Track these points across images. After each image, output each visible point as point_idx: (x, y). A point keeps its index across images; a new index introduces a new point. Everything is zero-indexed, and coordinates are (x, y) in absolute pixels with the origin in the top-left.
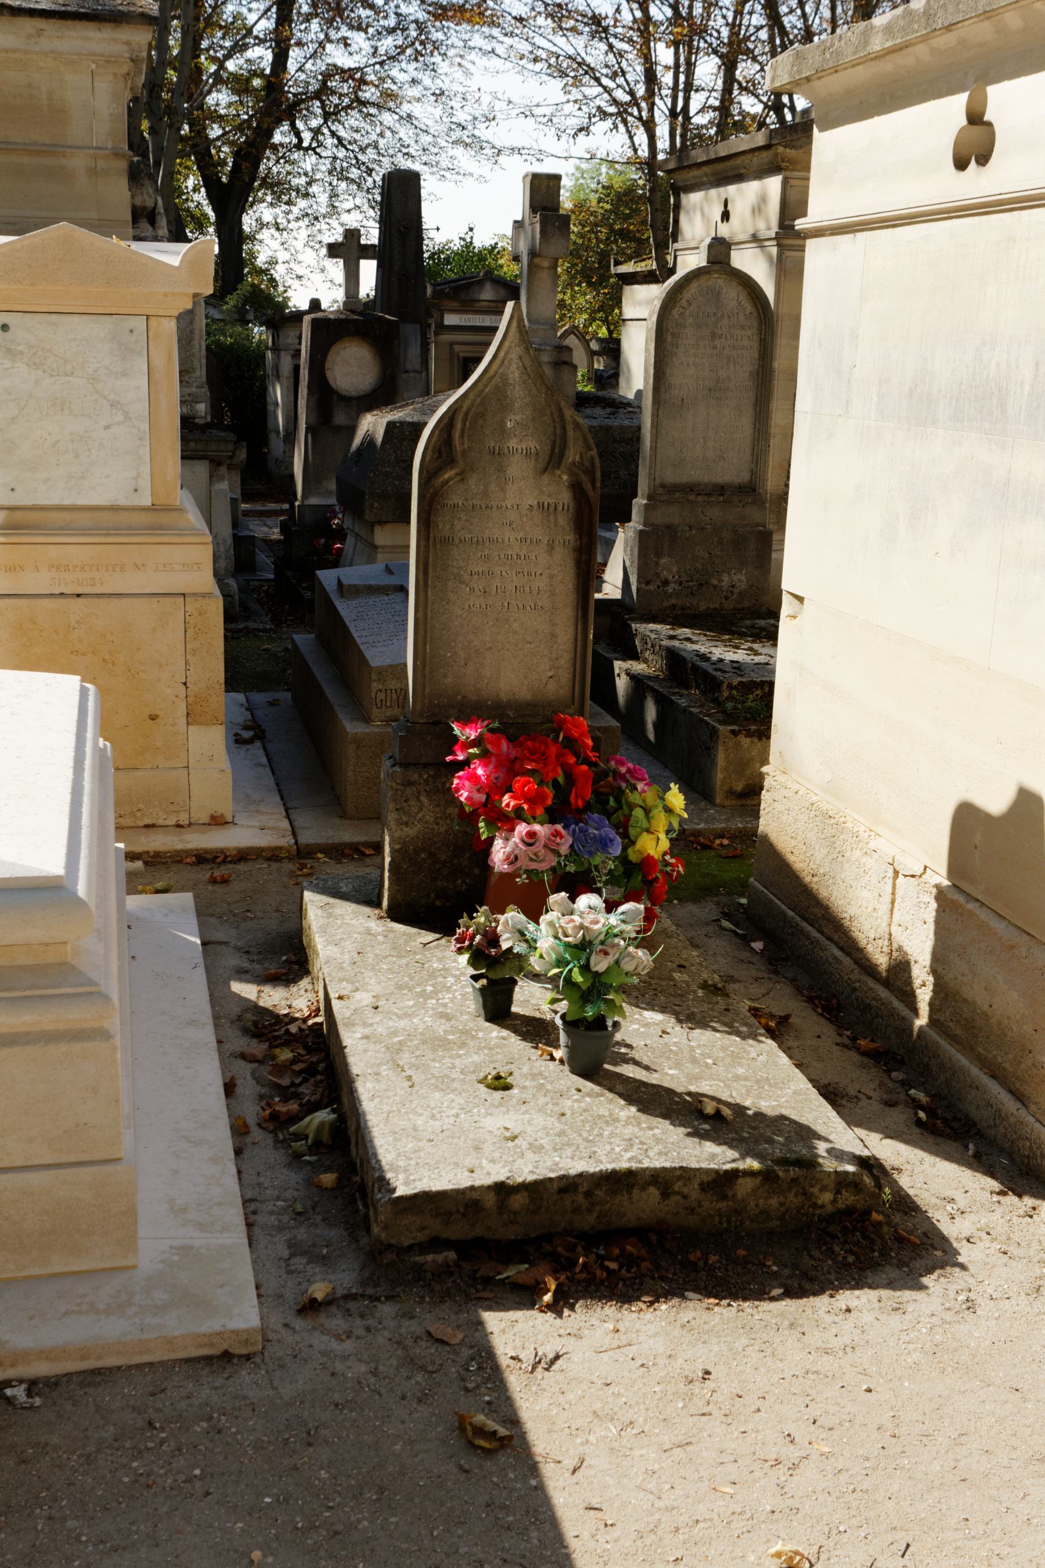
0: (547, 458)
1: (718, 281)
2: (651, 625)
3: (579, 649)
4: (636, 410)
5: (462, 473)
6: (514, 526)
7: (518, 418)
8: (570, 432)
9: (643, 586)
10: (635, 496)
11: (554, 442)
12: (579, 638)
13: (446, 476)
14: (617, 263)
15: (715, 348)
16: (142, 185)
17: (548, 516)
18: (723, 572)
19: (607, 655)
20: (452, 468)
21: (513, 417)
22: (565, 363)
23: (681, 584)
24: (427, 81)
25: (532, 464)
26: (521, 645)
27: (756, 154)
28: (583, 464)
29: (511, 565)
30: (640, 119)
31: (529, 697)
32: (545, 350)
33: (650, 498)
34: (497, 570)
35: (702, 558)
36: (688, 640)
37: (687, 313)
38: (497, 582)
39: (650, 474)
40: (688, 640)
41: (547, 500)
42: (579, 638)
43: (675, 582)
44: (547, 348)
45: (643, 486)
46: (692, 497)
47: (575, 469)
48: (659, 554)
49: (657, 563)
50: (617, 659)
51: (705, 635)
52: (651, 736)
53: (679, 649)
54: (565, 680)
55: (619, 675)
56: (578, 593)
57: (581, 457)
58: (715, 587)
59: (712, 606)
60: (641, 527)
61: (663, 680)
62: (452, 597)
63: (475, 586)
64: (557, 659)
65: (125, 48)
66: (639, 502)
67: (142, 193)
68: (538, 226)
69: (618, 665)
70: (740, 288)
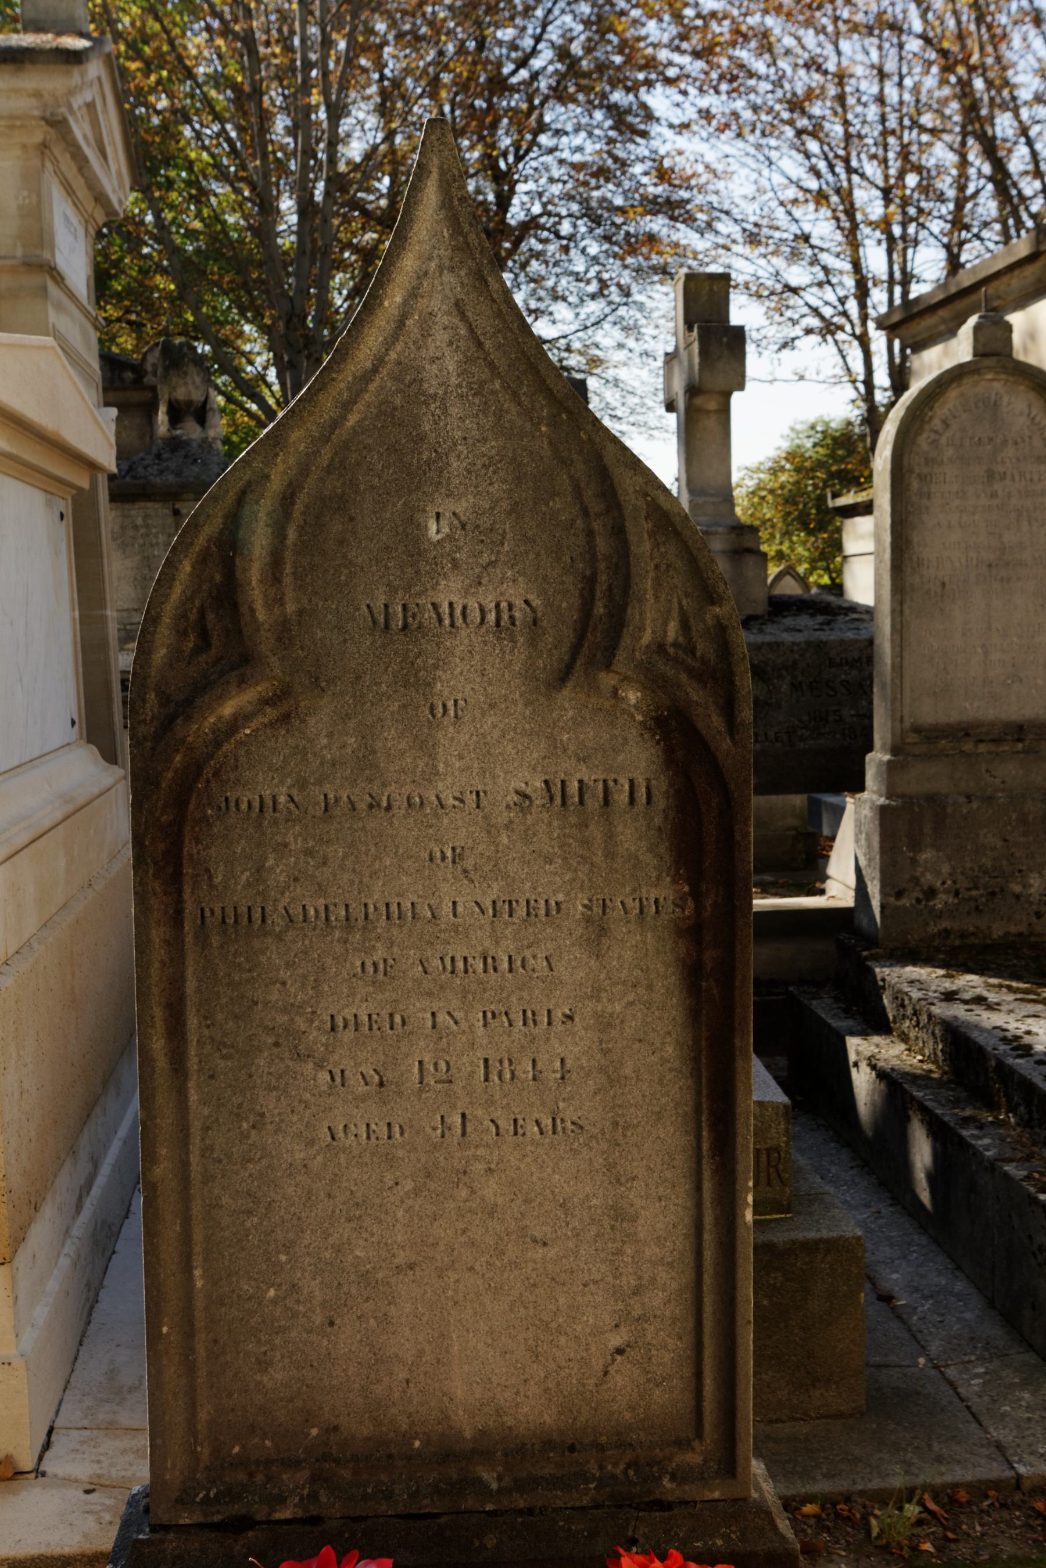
0: (568, 635)
1: (993, 385)
2: (909, 969)
3: (708, 1255)
4: (865, 617)
5: (282, 695)
6: (469, 863)
7: (463, 506)
8: (642, 546)
9: (892, 900)
10: (870, 748)
11: (590, 581)
12: (708, 1219)
13: (228, 709)
14: (835, 496)
15: (994, 495)
16: (186, 373)
17: (584, 825)
18: (1030, 870)
19: (835, 1023)
20: (242, 682)
21: (448, 507)
22: (749, 551)
23: (957, 894)
24: (631, 343)
25: (519, 657)
26: (512, 1251)
27: (1016, 272)
28: (692, 651)
29: (465, 992)
30: (853, 335)
31: (548, 1418)
32: (716, 533)
33: (895, 750)
34: (419, 1010)
35: (994, 849)
36: (980, 1000)
37: (943, 440)
38: (422, 1050)
39: (893, 711)
40: (980, 1000)
41: (577, 774)
42: (708, 1219)
43: (947, 892)
44: (720, 530)
45: (882, 731)
46: (968, 746)
47: (663, 667)
48: (916, 845)
49: (914, 861)
50: (853, 1034)
51: (1010, 988)
52: (925, 1197)
53: (968, 1025)
54: (667, 1357)
55: (856, 1064)
56: (696, 1073)
57: (685, 626)
58: (1018, 897)
59: (1013, 929)
60: (882, 801)
61: (940, 1083)
62: (270, 1103)
63: (347, 1064)
64: (637, 1292)
65: (33, 102)
66: (876, 760)
67: (186, 384)
68: (696, 347)
69: (856, 1046)
70: (1032, 395)
